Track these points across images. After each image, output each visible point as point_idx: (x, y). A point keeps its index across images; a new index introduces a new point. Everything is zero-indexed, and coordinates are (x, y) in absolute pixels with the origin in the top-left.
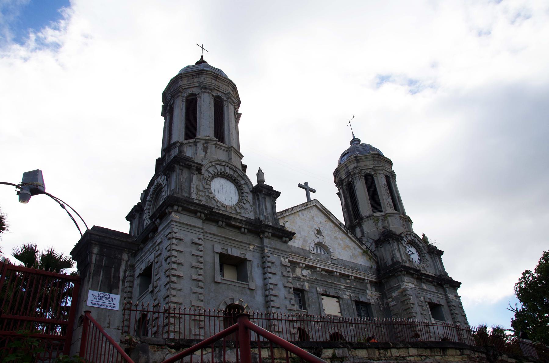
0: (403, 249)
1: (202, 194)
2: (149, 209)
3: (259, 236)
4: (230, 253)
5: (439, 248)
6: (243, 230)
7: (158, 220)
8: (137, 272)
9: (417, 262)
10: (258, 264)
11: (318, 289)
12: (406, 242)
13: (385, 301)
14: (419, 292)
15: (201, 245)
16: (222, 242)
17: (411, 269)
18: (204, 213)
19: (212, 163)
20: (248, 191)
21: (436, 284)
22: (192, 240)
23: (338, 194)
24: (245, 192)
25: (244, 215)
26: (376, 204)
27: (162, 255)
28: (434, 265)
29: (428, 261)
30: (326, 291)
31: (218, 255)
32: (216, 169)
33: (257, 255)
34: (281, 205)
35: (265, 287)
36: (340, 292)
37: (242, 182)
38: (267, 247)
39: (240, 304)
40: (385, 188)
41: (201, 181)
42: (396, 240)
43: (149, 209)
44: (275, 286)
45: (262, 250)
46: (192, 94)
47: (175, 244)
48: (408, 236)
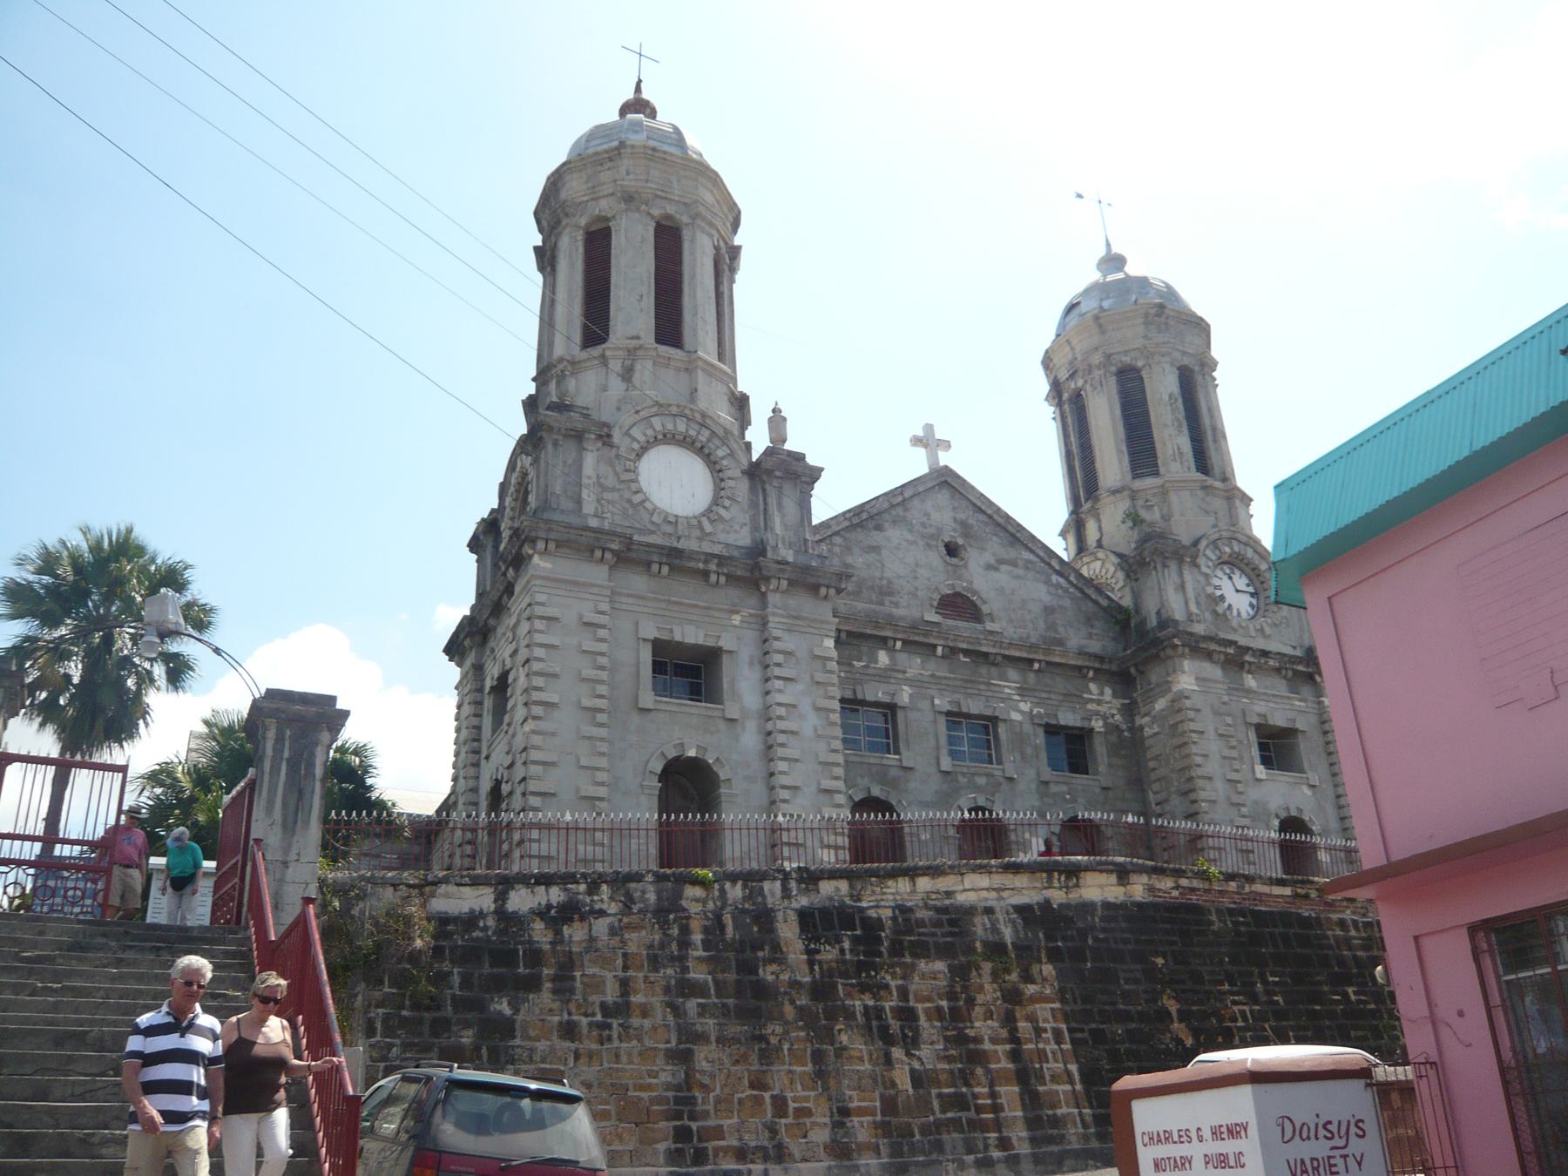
4: (678, 638)
7: (511, 570)
8: (488, 684)
11: (937, 701)
12: (1211, 560)
14: (1226, 698)
15: (604, 627)
19: (641, 413)
20: (737, 473)
22: (580, 616)
25: (722, 537)
27: (519, 653)
30: (959, 704)
31: (1253, 728)
32: (652, 427)
33: (751, 635)
34: (827, 503)
35: (766, 714)
39: (700, 756)
40: (1171, 404)
41: (611, 464)
44: (790, 709)
45: (764, 624)
47: (541, 632)
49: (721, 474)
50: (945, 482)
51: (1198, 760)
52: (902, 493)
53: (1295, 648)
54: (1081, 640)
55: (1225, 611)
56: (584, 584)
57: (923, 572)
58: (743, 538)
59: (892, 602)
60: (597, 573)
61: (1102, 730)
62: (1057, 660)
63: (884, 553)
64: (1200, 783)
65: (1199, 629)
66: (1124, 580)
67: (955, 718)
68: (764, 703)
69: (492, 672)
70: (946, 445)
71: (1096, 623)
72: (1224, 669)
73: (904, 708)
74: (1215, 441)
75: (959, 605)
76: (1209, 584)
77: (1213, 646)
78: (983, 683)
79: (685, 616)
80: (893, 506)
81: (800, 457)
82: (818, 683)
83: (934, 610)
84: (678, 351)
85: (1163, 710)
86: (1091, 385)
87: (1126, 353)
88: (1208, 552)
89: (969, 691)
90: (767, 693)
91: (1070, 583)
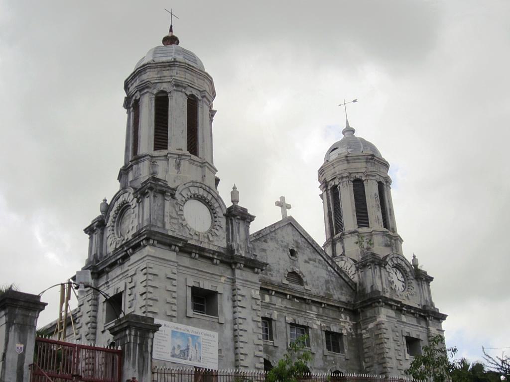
0: (385, 275)
1: (175, 221)
2: (113, 226)
3: (231, 266)
4: (202, 287)
5: (429, 274)
6: (215, 261)
7: (131, 250)
9: (400, 290)
10: (228, 296)
11: (287, 318)
13: (359, 331)
14: (396, 325)
15: (175, 280)
16: (194, 274)
17: (392, 300)
18: (178, 246)
19: (186, 185)
21: (418, 315)
22: (166, 275)
23: (321, 196)
24: (219, 217)
25: (216, 243)
26: (362, 218)
28: (420, 293)
29: (413, 288)
30: (295, 320)
31: (190, 289)
33: (228, 287)
35: (234, 321)
36: (310, 321)
37: (216, 205)
38: (238, 279)
40: (375, 198)
41: (174, 207)
42: (378, 265)
43: (113, 226)
44: (244, 320)
45: (233, 281)
46: (163, 92)
48: (394, 260)
49: (215, 215)
50: (291, 223)
51: (387, 350)
52: (274, 227)
53: (419, 305)
54: (340, 296)
56: (167, 260)
57: (282, 262)
58: (224, 244)
59: (270, 274)
60: (171, 256)
61: (346, 334)
62: (331, 303)
63: (268, 252)
64: (388, 360)
65: (387, 295)
66: (355, 271)
67: (328, 333)
68: (233, 317)
70: (289, 207)
71: (344, 288)
72: (396, 313)
73: (275, 320)
75: (295, 276)
76: (389, 276)
77: (393, 303)
78: (304, 312)
79: (204, 277)
80: (271, 232)
81: (245, 210)
82: (254, 310)
83: (285, 279)
84: (197, 157)
85: (372, 328)
86: (342, 185)
89: (298, 315)
90: (234, 313)
91: (335, 270)
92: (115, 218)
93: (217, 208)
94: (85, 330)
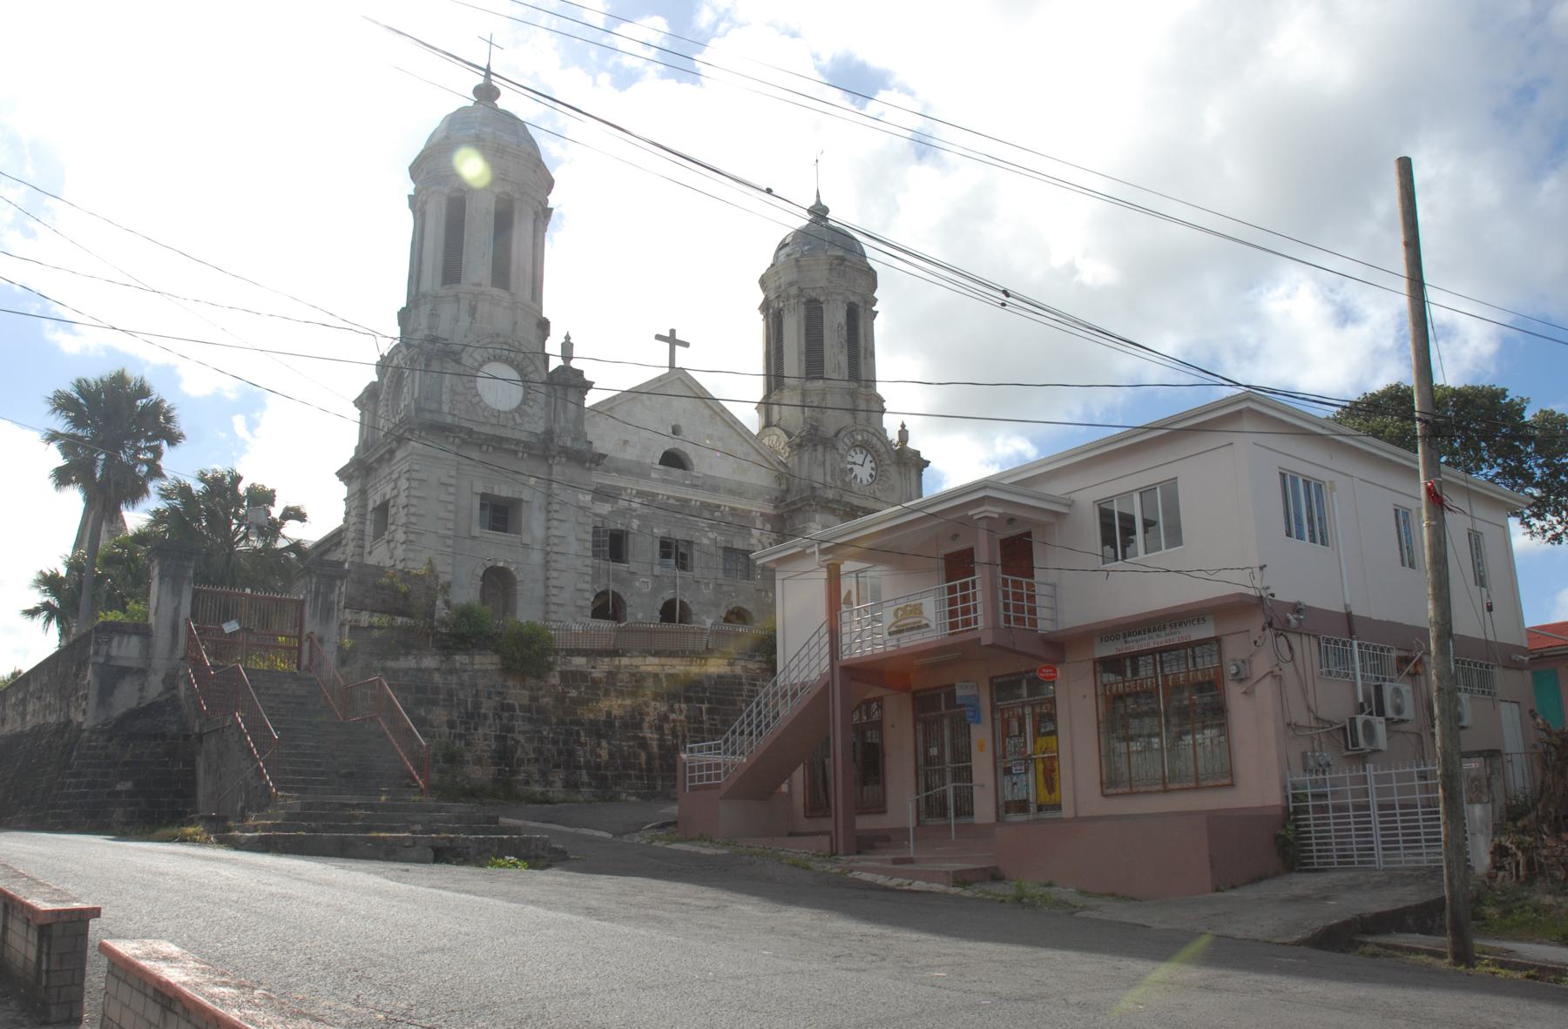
4: (496, 492)
31: (479, 497)
36: (697, 534)
43: (387, 400)
47: (415, 488)
55: (851, 480)
58: (540, 428)
69: (374, 500)
74: (865, 358)
82: (580, 523)
87: (814, 289)
88: (846, 439)
90: (548, 528)
92: (389, 387)
93: (531, 373)
94: (350, 548)
